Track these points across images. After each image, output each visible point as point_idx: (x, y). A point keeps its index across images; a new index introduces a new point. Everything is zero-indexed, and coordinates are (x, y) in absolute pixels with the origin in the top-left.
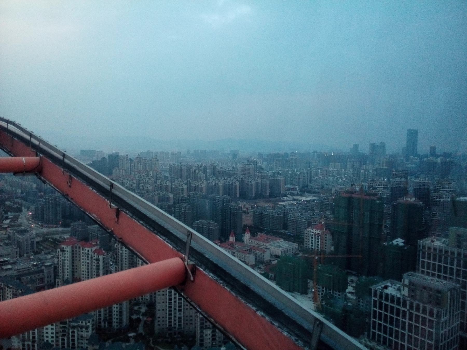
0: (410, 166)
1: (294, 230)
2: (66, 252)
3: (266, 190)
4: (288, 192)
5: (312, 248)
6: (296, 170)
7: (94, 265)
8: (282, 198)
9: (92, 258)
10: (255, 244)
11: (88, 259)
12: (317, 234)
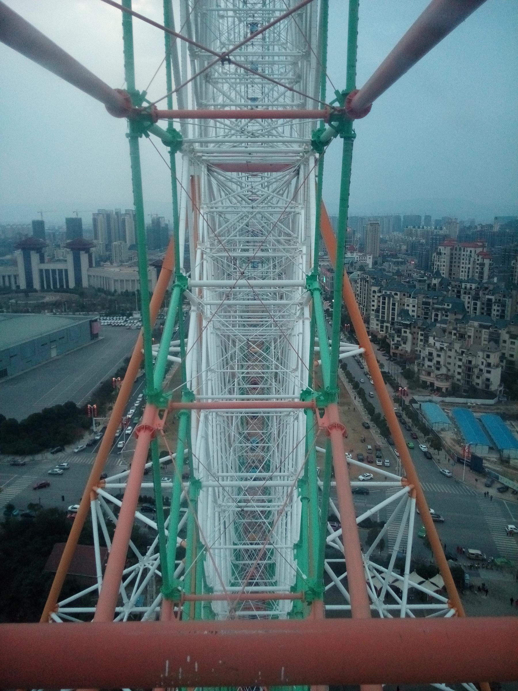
2: (443, 256)
7: (477, 272)
9: (474, 262)
11: (469, 263)
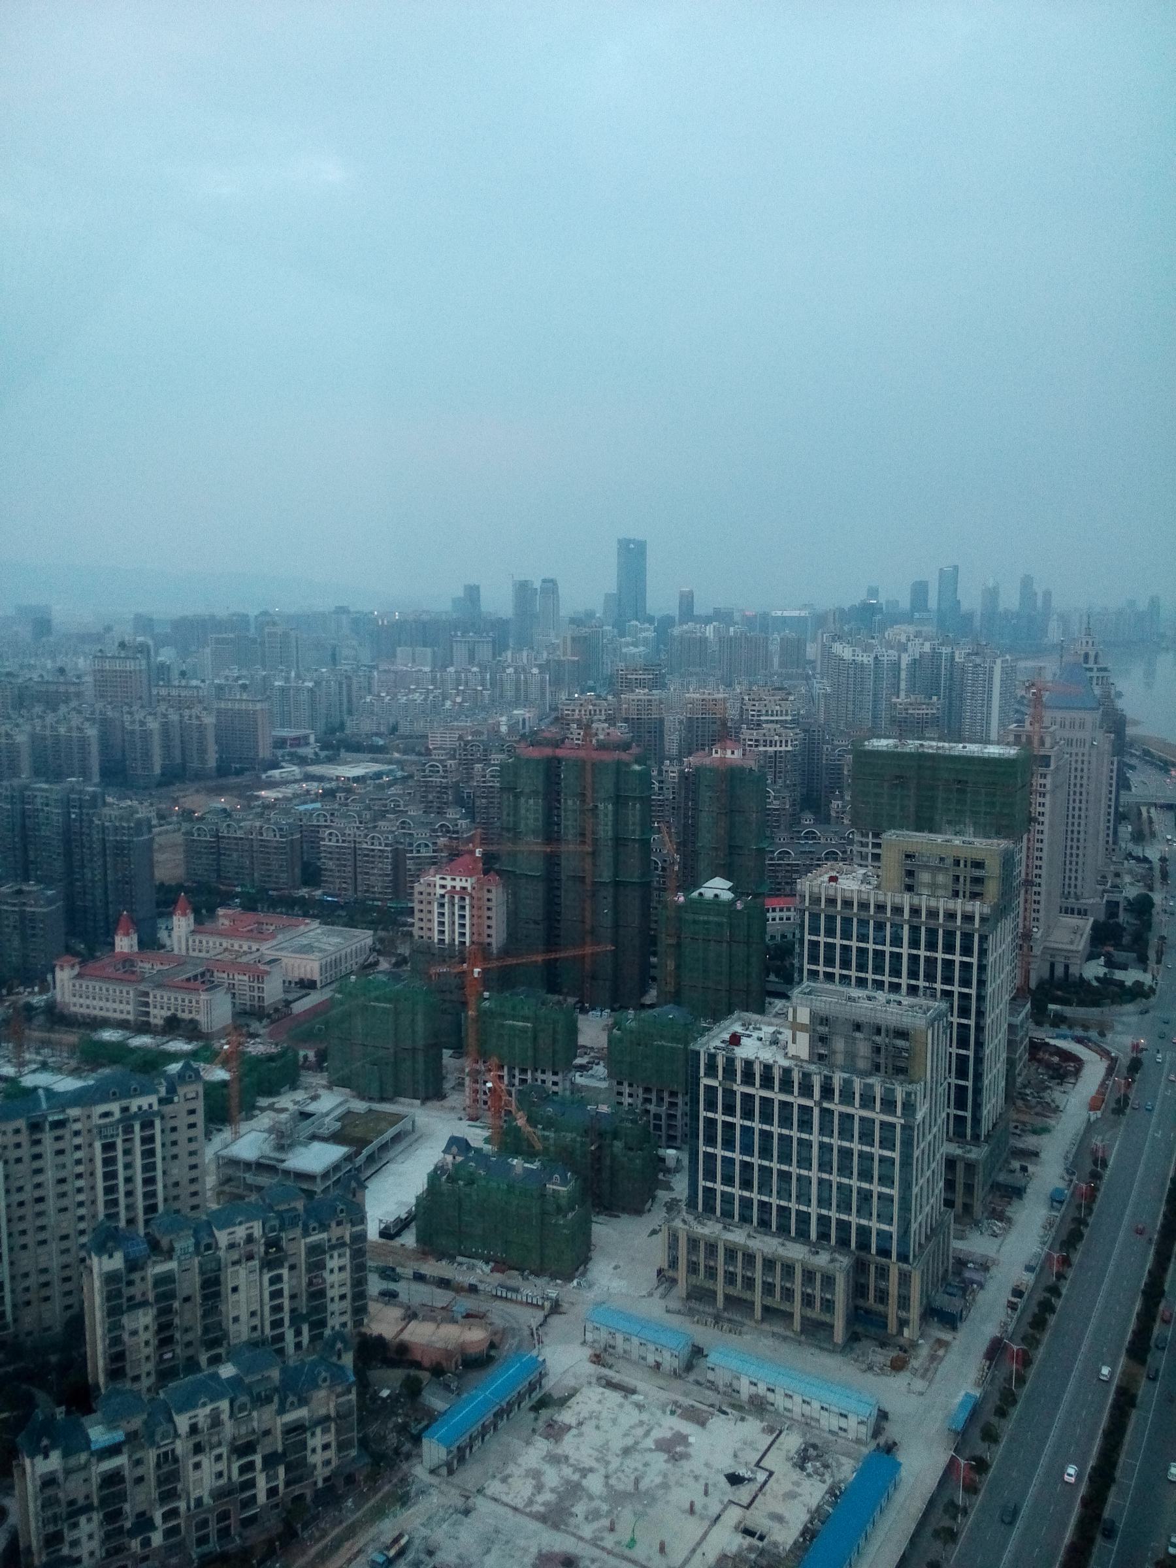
0: (633, 650)
1: (344, 885)
3: (202, 751)
4: (279, 752)
5: (442, 941)
6: (293, 674)
8: (264, 776)
10: (218, 951)
12: (457, 893)
